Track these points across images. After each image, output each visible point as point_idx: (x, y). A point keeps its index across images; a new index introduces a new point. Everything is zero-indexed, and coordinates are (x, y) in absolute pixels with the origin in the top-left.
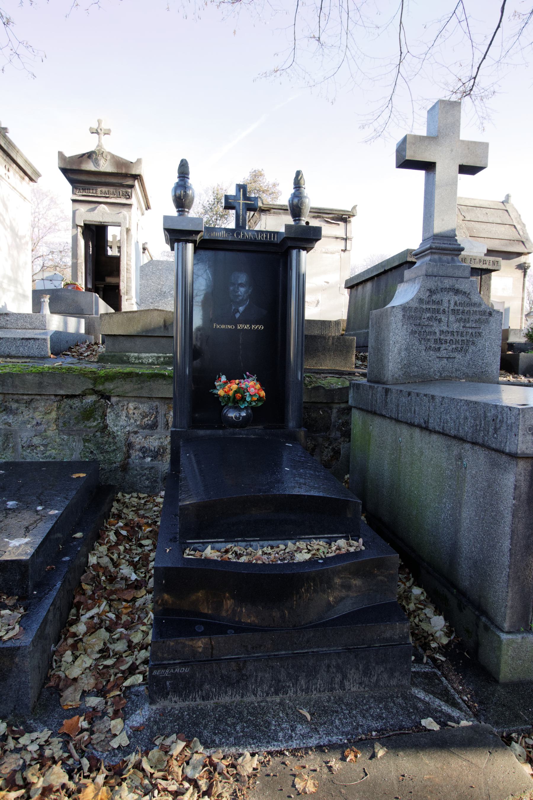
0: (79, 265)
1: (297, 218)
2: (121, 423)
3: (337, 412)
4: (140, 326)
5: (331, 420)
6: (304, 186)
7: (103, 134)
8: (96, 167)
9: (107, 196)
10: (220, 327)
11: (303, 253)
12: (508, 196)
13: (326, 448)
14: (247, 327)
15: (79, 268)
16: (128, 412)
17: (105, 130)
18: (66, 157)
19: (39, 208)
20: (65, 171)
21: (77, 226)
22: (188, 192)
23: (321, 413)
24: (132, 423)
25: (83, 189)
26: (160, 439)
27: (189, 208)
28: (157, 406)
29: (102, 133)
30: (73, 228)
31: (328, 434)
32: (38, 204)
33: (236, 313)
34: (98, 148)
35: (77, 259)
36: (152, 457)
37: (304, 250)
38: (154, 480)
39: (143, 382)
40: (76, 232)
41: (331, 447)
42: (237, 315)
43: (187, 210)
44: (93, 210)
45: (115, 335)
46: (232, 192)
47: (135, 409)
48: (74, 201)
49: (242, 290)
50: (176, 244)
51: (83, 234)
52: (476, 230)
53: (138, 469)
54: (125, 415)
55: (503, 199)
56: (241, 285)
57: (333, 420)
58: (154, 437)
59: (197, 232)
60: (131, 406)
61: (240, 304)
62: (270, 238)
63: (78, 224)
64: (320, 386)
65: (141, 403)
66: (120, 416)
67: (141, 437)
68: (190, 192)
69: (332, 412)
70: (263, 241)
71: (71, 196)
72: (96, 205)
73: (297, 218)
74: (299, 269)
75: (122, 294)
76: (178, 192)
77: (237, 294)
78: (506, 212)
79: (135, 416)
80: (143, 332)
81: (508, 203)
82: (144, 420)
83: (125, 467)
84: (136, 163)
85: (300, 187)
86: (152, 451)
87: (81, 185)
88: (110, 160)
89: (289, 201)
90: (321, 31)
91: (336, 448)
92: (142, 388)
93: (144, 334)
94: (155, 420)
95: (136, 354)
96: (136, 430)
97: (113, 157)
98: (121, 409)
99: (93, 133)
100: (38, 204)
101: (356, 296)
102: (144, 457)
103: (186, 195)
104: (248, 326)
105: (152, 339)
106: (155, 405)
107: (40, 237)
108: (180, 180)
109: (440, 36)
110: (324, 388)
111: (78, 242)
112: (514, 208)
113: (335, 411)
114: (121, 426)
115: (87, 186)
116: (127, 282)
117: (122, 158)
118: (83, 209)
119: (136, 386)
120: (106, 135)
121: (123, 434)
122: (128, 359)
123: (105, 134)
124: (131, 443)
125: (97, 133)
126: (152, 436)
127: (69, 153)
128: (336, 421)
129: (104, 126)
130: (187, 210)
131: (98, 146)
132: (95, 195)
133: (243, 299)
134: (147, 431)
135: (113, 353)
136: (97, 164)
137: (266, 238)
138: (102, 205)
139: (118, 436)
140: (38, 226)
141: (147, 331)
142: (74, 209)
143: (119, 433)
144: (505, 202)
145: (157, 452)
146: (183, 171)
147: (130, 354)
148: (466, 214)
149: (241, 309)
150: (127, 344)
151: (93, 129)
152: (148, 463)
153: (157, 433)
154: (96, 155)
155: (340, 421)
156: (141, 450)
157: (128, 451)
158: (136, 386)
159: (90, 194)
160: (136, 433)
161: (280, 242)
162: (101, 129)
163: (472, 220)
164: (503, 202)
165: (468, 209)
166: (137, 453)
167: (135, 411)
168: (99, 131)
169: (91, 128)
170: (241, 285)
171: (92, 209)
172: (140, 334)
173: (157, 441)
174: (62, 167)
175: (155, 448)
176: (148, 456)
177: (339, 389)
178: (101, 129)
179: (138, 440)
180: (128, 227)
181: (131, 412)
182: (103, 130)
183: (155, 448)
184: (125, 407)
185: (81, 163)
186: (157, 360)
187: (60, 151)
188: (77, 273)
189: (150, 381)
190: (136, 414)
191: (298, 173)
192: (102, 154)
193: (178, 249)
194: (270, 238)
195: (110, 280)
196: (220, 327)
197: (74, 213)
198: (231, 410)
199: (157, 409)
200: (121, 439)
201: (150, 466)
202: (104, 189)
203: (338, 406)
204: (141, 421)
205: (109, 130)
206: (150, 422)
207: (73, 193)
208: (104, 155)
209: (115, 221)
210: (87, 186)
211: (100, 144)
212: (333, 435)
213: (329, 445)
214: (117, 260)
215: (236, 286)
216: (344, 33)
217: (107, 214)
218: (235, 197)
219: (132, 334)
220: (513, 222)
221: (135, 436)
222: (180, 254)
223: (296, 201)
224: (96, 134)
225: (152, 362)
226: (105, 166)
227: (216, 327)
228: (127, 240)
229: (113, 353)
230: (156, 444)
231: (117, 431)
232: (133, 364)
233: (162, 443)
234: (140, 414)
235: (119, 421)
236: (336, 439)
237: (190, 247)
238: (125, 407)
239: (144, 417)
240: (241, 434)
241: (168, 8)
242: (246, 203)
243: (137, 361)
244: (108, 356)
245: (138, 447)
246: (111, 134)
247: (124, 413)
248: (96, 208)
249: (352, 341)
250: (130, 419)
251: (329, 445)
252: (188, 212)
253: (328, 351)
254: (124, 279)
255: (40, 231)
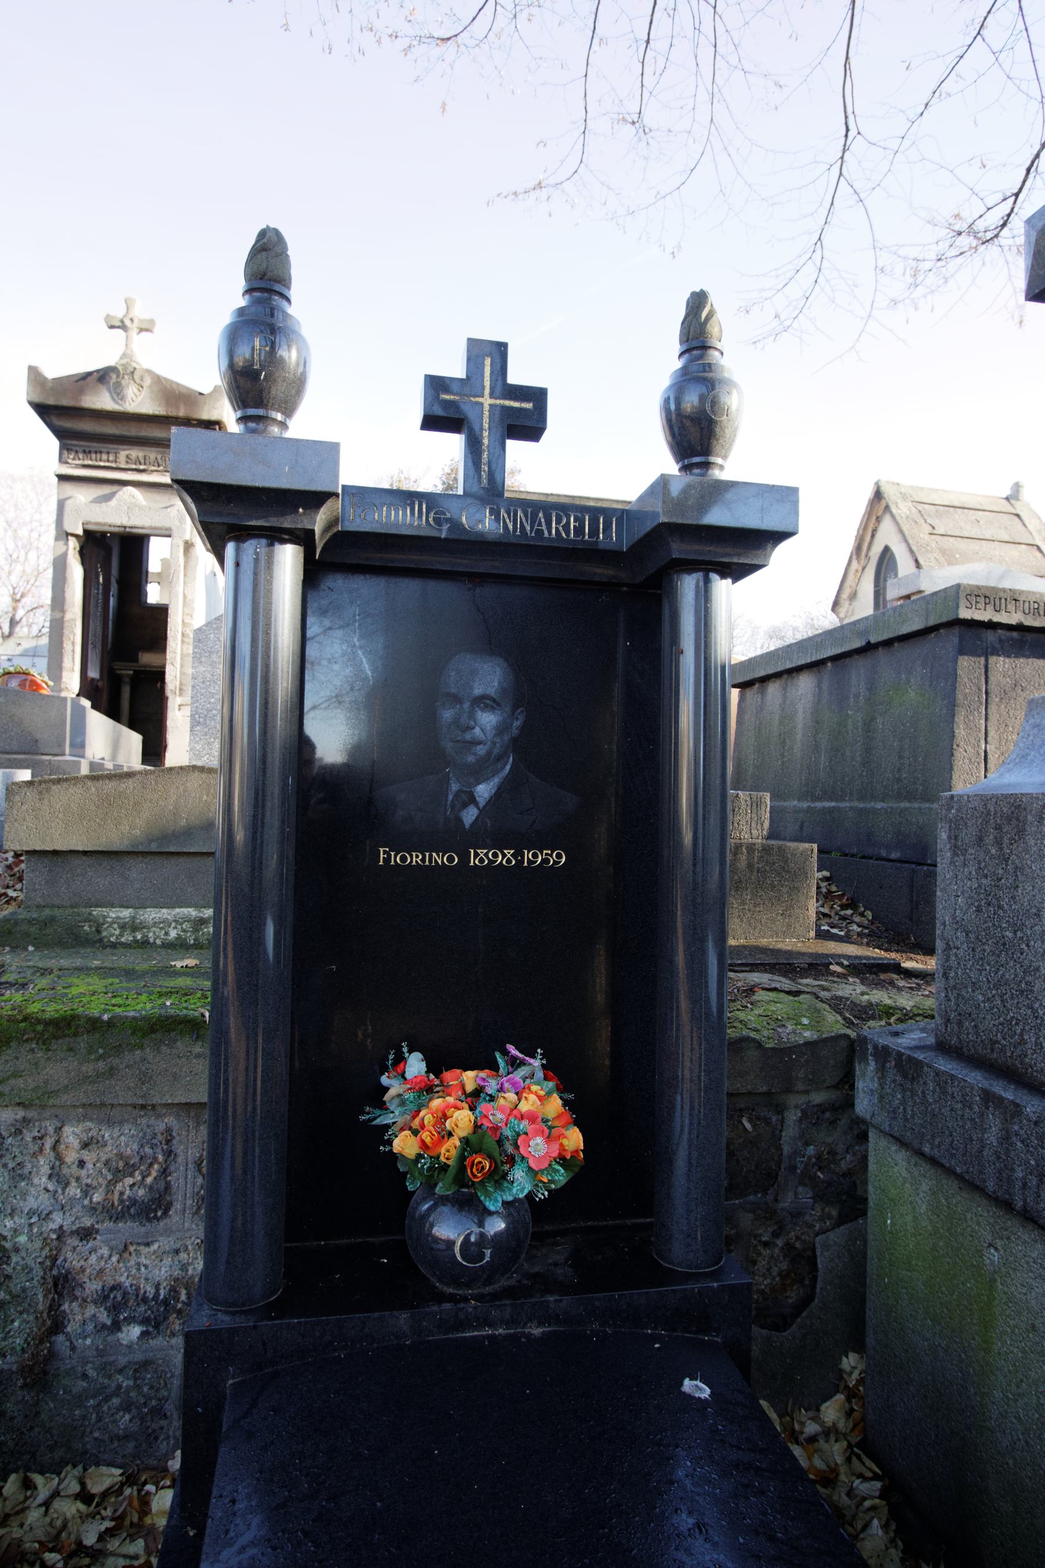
0: (66, 624)
1: (696, 460)
2: (31, 1203)
3: (800, 1120)
4: (140, 823)
5: (779, 1148)
6: (718, 345)
7: (136, 331)
8: (117, 403)
9: (142, 467)
10: (403, 859)
11: (722, 588)
12: (1017, 487)
13: (766, 1244)
14: (505, 857)
15: (66, 632)
16: (59, 1157)
17: (141, 321)
18: (46, 378)
19: (40, 513)
20: (43, 410)
21: (68, 534)
22: (282, 352)
23: (748, 1126)
24: (72, 1199)
25: (84, 452)
26: (177, 1252)
27: (289, 411)
28: (169, 1131)
29: (133, 328)
30: (57, 539)
31: (770, 1198)
32: (40, 505)
33: (465, 805)
34: (124, 361)
35: (63, 611)
36: (145, 1321)
37: (723, 576)
38: (152, 1411)
39: (118, 1050)
40: (64, 548)
41: (780, 1242)
42: (470, 815)
43: (279, 417)
44: (107, 498)
45: (55, 853)
46: (455, 369)
47: (85, 1145)
48: (62, 478)
49: (488, 720)
50: (230, 548)
51: (82, 553)
52: (960, 554)
53: (92, 1373)
54: (45, 1170)
55: (1007, 492)
56: (484, 702)
57: (786, 1149)
58: (155, 1246)
59: (316, 499)
60: (72, 1135)
61: (479, 772)
62: (594, 532)
63: (70, 531)
64: (748, 1039)
65: (110, 1123)
66: (27, 1178)
67: (105, 1251)
68: (290, 355)
69: (782, 1121)
70: (568, 541)
71: (55, 467)
72: (114, 488)
73: (696, 460)
74: (707, 646)
75: (169, 692)
76: (243, 353)
77: (468, 736)
78: (1016, 518)
79: (84, 1173)
80: (150, 841)
81: (1017, 499)
82: (119, 1187)
83: (40, 1371)
84: (210, 394)
85: (705, 347)
86: (145, 1300)
87: (81, 443)
88: (150, 386)
89: (667, 401)
90: (646, 94)
91: (798, 1245)
92: (112, 1071)
93: (154, 847)
94: (162, 1185)
95: (126, 913)
96: (87, 1222)
97: (158, 380)
98: (33, 1148)
99: (112, 327)
100: (40, 505)
101: (761, 708)
102: (116, 1326)
103: (272, 358)
104: (509, 853)
105: (184, 863)
106: (162, 1127)
107: (41, 569)
108: (255, 302)
109: (937, 93)
110: (759, 1045)
111: (68, 571)
112: (1031, 510)
113: (792, 1116)
114: (31, 1213)
115: (95, 445)
116: (182, 666)
117: (178, 384)
118: (81, 496)
119: (88, 1068)
120: (144, 334)
121: (38, 1244)
122: (99, 932)
123: (141, 330)
124: (68, 1272)
125: (123, 327)
126: (148, 1244)
127: (52, 372)
128: (796, 1153)
129: (140, 312)
130: (279, 417)
131: (124, 355)
132: (114, 465)
133: (489, 753)
134: (128, 1228)
135: (47, 912)
136: (118, 395)
137: (579, 531)
138: (130, 489)
139: (17, 1250)
140: (38, 548)
141: (165, 837)
142: (61, 497)
143: (22, 1239)
144: (1013, 497)
145: (166, 1302)
146: (267, 272)
147: (105, 911)
148: (935, 522)
149: (484, 791)
150: (100, 879)
151: (113, 317)
152: (130, 1346)
153: (168, 1232)
154: (118, 376)
155: (811, 1150)
156: (106, 1298)
157: (54, 1307)
158: (88, 1068)
159: (102, 464)
160: (86, 1234)
161: (630, 549)
162: (132, 320)
163: (949, 533)
164: (1007, 499)
165: (937, 511)
166: (91, 1310)
167: (86, 1155)
168: (128, 322)
169: (108, 316)
170: (484, 702)
171: (104, 496)
172: (141, 849)
173: (168, 1261)
174: (37, 400)
175: (157, 1286)
176: (131, 1320)
177: (808, 1044)
178: (132, 320)
179: (95, 1262)
180: (188, 537)
181: (71, 1157)
182: (136, 321)
183: (157, 1286)
184: (49, 1143)
185: (81, 391)
186: (196, 930)
187: (33, 364)
188: (62, 643)
189: (142, 1048)
190: (90, 1166)
191: (698, 302)
192: (133, 373)
193: (237, 564)
194: (594, 532)
195: (147, 658)
196: (403, 859)
197: (61, 505)
198: (445, 1209)
199: (168, 1142)
200: (30, 1261)
201: (139, 1357)
202: (135, 453)
203: (802, 1099)
204: (109, 1191)
205: (152, 322)
206: (141, 1192)
207: (62, 460)
208: (137, 376)
209: (158, 525)
210: (95, 444)
211: (129, 352)
212: (787, 1202)
213: (776, 1235)
214: (161, 612)
215: (466, 705)
216: (703, 96)
217: (141, 508)
218: (470, 383)
219: (115, 849)
220: (1033, 539)
221: (85, 1247)
222: (247, 583)
223: (691, 400)
224: (120, 331)
225: (179, 937)
226: (138, 400)
227: (387, 860)
228: (185, 567)
229: (47, 912)
230: (163, 1272)
231: (16, 1231)
232: (114, 946)
233: (184, 1267)
234: (107, 1163)
235: (24, 1195)
236: (797, 1214)
237: (288, 559)
238: (49, 1143)
239: (118, 1174)
240: (487, 1322)
241: (287, 24)
242: (504, 408)
243: (127, 938)
244: (30, 922)
245: (93, 1287)
246: (155, 330)
247: (44, 1165)
248: (114, 494)
249: (806, 855)
250: (67, 1184)
251: (776, 1235)
252: (283, 425)
253: (737, 889)
254: (175, 658)
255: (42, 558)
